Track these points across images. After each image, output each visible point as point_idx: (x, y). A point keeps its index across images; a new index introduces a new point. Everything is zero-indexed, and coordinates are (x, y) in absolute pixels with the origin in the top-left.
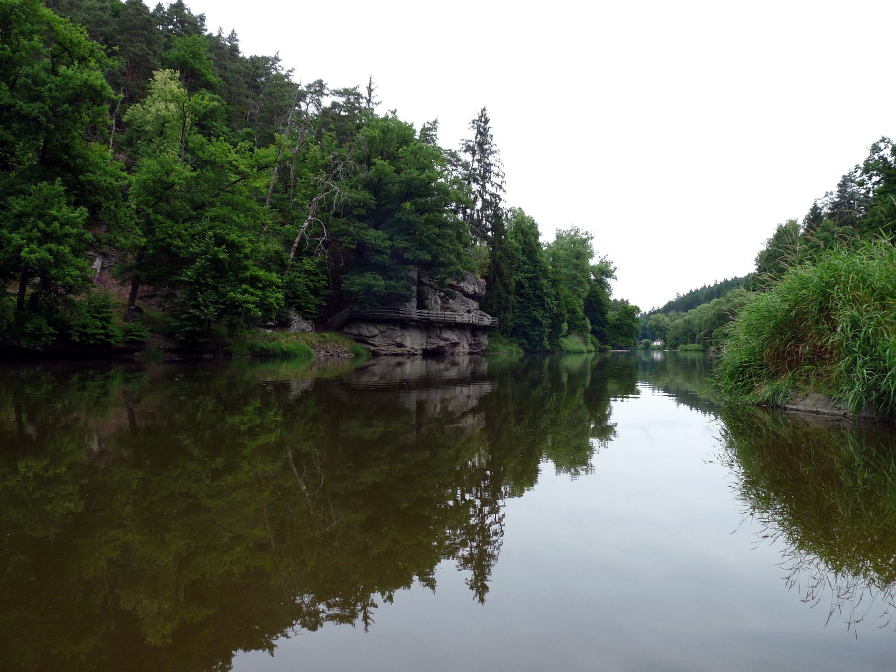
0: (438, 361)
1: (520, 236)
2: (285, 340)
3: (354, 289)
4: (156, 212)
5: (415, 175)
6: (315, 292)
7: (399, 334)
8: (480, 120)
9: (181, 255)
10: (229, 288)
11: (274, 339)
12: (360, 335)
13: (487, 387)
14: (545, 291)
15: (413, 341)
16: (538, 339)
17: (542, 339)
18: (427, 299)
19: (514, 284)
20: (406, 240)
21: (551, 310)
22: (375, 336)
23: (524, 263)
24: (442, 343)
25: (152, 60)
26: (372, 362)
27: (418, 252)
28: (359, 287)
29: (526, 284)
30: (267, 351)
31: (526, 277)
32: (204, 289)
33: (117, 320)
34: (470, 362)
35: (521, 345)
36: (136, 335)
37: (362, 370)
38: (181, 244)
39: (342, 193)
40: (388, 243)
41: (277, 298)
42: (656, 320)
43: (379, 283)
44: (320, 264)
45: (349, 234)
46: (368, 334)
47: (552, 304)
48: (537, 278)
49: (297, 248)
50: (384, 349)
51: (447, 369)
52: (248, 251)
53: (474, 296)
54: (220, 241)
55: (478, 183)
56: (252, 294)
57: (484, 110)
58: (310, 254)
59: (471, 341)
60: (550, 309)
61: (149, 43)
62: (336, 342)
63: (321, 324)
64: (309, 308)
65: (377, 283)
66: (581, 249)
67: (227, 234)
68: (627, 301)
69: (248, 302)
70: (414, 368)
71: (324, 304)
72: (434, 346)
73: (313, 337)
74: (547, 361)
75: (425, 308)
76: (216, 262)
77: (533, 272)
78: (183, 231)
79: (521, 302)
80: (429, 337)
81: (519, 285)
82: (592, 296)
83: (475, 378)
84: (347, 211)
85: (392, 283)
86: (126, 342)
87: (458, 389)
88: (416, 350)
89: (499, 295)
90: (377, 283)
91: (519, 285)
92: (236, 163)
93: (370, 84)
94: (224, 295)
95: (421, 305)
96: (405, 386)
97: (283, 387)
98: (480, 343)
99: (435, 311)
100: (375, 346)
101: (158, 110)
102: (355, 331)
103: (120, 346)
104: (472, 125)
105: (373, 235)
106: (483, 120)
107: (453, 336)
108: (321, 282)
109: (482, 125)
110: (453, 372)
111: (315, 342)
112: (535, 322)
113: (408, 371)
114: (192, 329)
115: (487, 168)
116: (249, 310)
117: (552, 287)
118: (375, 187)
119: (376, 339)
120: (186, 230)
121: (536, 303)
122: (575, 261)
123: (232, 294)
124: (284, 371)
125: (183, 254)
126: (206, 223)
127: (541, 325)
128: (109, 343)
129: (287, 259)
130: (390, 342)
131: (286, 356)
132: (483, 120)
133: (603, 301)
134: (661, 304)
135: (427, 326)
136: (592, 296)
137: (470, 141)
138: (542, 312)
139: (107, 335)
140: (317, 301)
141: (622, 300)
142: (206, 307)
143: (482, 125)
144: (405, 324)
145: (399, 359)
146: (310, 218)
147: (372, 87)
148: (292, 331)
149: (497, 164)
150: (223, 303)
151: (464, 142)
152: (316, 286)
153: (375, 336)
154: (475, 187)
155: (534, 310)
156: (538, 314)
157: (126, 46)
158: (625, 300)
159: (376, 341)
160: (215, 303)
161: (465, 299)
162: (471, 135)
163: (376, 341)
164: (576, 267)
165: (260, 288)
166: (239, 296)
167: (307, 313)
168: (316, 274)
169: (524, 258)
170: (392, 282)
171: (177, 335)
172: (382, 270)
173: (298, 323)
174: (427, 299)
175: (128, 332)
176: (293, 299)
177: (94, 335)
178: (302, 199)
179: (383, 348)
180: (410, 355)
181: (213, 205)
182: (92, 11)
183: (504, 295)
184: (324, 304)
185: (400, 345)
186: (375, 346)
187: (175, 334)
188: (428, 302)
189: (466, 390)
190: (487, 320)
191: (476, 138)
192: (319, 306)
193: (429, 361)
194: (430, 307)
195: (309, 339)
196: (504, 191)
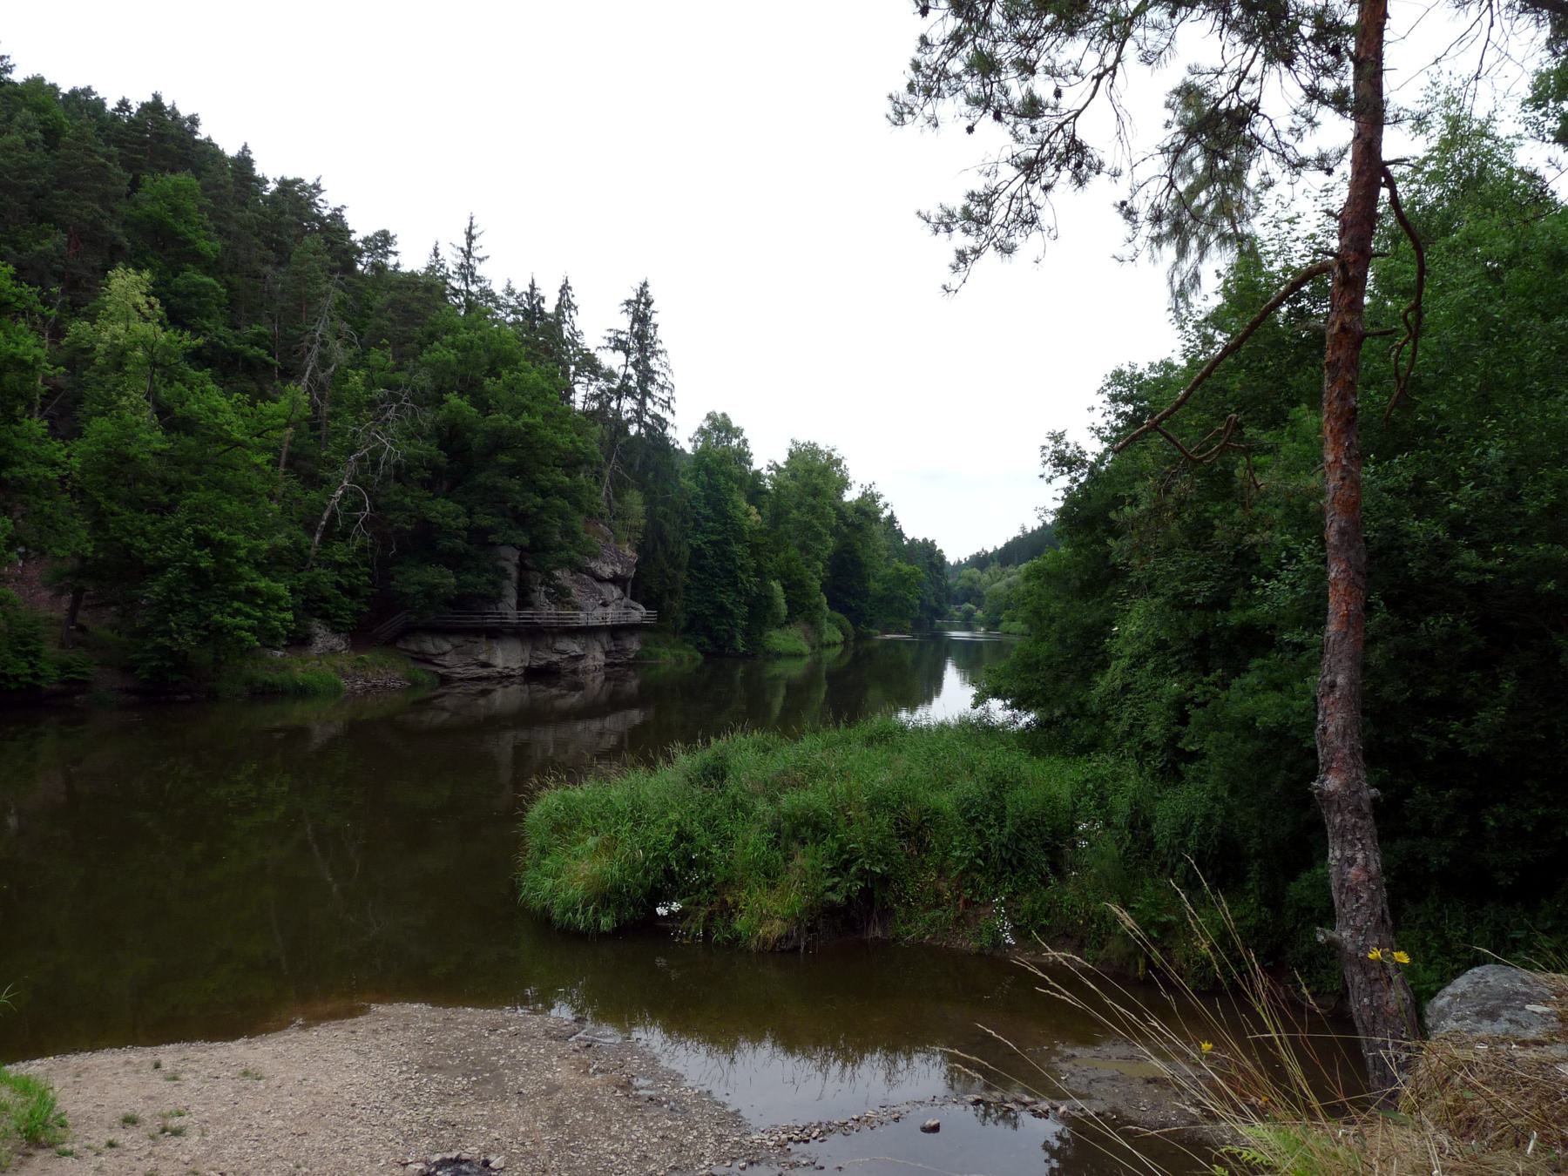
0: (550, 685)
1: (703, 477)
2: (301, 668)
3: (411, 590)
4: (110, 498)
5: (504, 422)
6: (352, 592)
7: (484, 648)
8: (638, 302)
9: (146, 562)
10: (213, 607)
11: (284, 668)
12: (422, 652)
13: (636, 716)
14: (739, 562)
15: (508, 657)
16: (726, 637)
17: (733, 637)
18: (534, 591)
19: (688, 553)
20: (493, 515)
21: (748, 593)
22: (444, 654)
23: (707, 519)
24: (555, 658)
25: (108, 227)
26: (441, 691)
27: (509, 532)
28: (417, 588)
29: (709, 552)
30: (273, 685)
31: (709, 542)
32: (178, 608)
33: (49, 649)
34: (607, 679)
35: (699, 646)
36: (78, 673)
37: (423, 704)
38: (146, 546)
39: (393, 449)
40: (463, 521)
41: (283, 621)
42: (971, 579)
43: (445, 579)
44: (362, 549)
45: (403, 508)
46: (434, 651)
47: (750, 582)
48: (727, 542)
49: (326, 528)
50: (459, 671)
51: (562, 696)
52: (242, 553)
53: (616, 580)
54: (203, 541)
55: (634, 398)
56: (248, 616)
57: (645, 285)
58: (345, 536)
59: (611, 646)
60: (746, 590)
61: (103, 198)
62: (381, 666)
63: (361, 635)
64: (341, 617)
65: (445, 581)
66: (820, 481)
67: (214, 530)
68: (933, 542)
69: (242, 628)
70: (506, 698)
71: (366, 609)
72: (542, 663)
73: (345, 658)
74: (739, 673)
75: (531, 605)
76: (196, 573)
77: (720, 533)
78: (149, 527)
79: (700, 579)
80: (535, 649)
81: (697, 553)
82: (846, 552)
83: (615, 704)
84: (401, 473)
85: (470, 578)
86: (64, 682)
87: (580, 727)
88: (513, 670)
89: (662, 571)
90: (445, 581)
91: (697, 553)
92: (229, 428)
93: (471, 228)
94: (208, 617)
95: (524, 602)
96: (495, 723)
97: (300, 733)
98: (624, 649)
99: (547, 611)
100: (445, 667)
101: (115, 337)
102: (413, 647)
103: (54, 687)
104: (625, 307)
105: (443, 509)
106: (643, 300)
107: (574, 647)
108: (361, 578)
109: (641, 310)
110: (574, 699)
111: (348, 669)
112: (722, 610)
113: (498, 703)
114: (160, 663)
115: (647, 376)
116: (241, 640)
117: (752, 555)
118: (451, 437)
119: (447, 658)
120: (153, 524)
121: (725, 581)
122: (810, 499)
123: (217, 617)
124: (298, 713)
125: (149, 560)
126: (182, 516)
127: (731, 614)
128: (39, 687)
129: (309, 548)
130: (470, 660)
131: (303, 692)
132: (643, 300)
133: (864, 558)
134: (995, 540)
135: (531, 634)
136: (846, 552)
137: (622, 333)
138: (734, 595)
139: (35, 676)
140: (355, 605)
141: (925, 540)
142: (181, 633)
143: (641, 310)
144: (495, 634)
145: (484, 685)
146: (346, 483)
147: (474, 232)
148: (314, 651)
149: (663, 370)
150: (206, 628)
151: (611, 335)
152: (351, 584)
153: (444, 654)
154: (628, 404)
155: (721, 592)
156: (727, 599)
157: (67, 207)
158: (930, 540)
159: (447, 660)
160: (195, 627)
161: (598, 586)
162: (624, 323)
163: (447, 660)
164: (813, 509)
165: (258, 606)
166: (229, 620)
167: (337, 623)
168: (354, 565)
169: (708, 512)
170: (469, 576)
171: (139, 671)
172: (454, 561)
173: (324, 639)
174: (534, 591)
175: (65, 668)
176: (312, 605)
177: (16, 678)
178: (335, 453)
179: (459, 670)
180: (503, 677)
181: (193, 486)
182: (14, 153)
183: (670, 571)
184: (366, 609)
185: (485, 665)
186: (445, 667)
187: (136, 669)
188: (533, 596)
189: (596, 725)
190: (638, 614)
191: (632, 328)
192: (357, 613)
193: (534, 686)
194: (538, 604)
195: (339, 664)
196: (673, 412)
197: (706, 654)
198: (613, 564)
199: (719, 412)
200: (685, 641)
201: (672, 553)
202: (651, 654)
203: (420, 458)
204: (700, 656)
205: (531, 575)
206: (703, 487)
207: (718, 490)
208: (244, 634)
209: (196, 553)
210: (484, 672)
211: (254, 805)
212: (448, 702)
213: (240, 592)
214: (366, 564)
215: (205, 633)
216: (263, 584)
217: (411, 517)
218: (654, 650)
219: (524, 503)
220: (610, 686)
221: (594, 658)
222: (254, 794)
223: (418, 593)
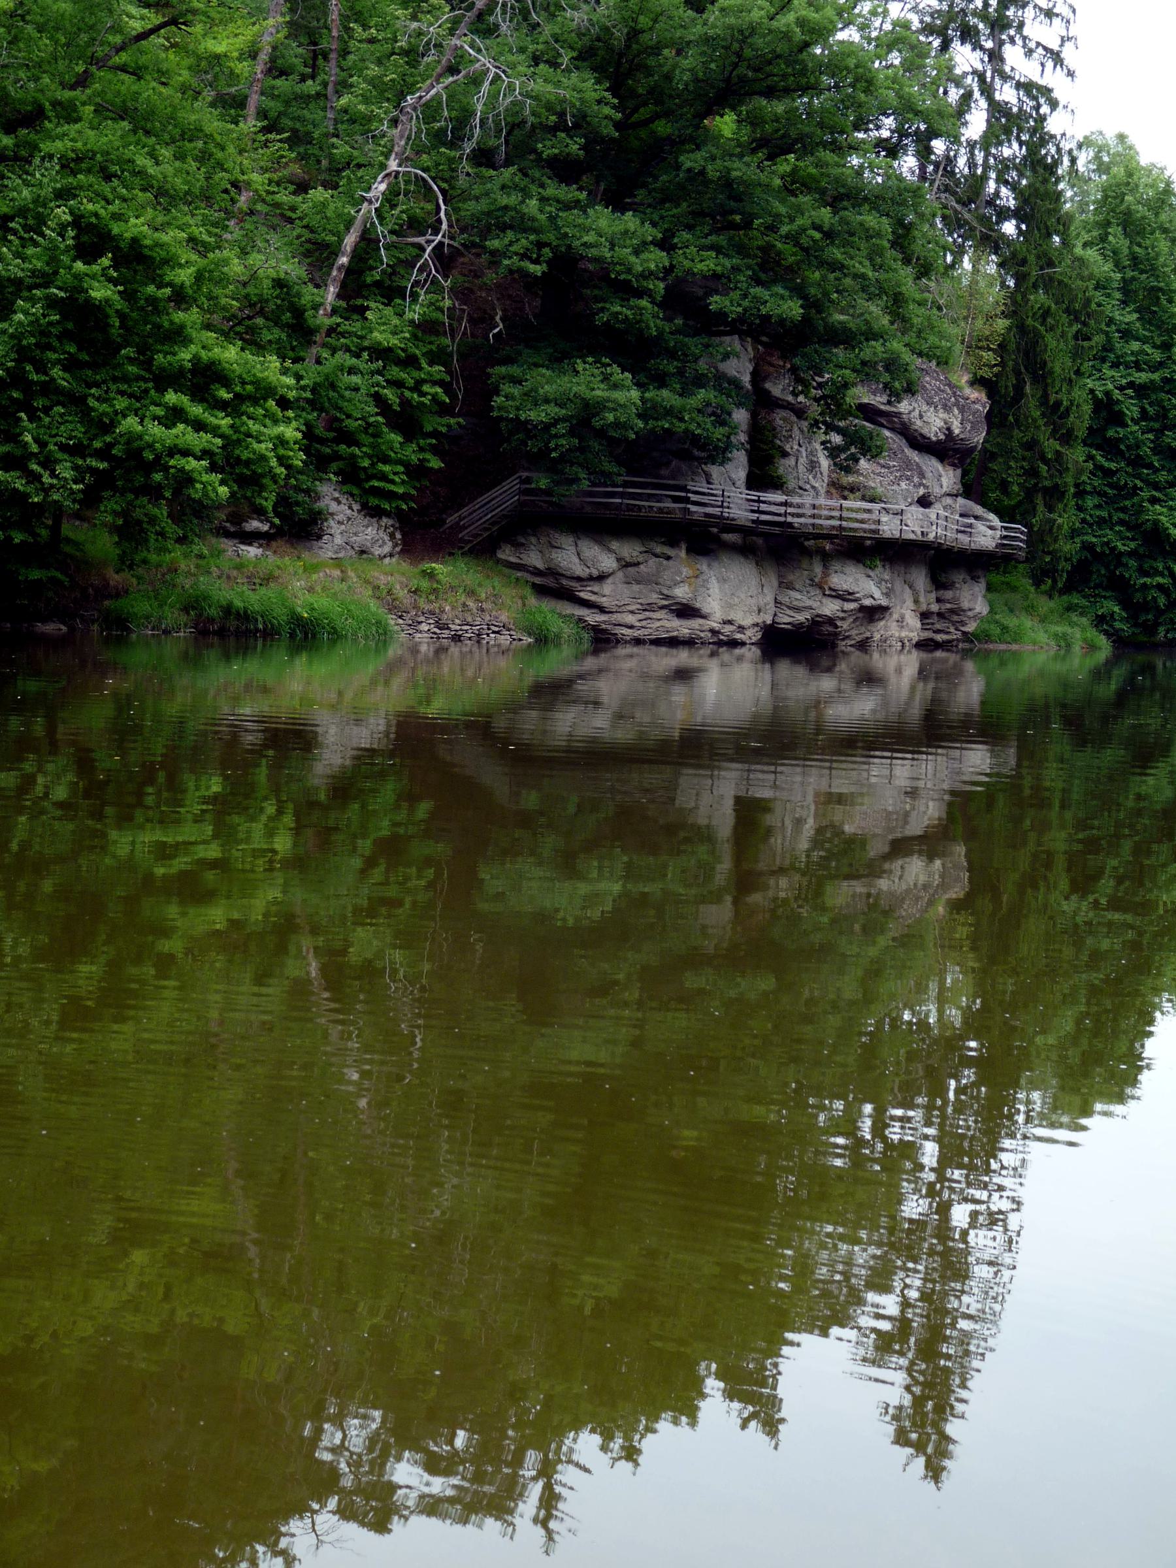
0: (814, 667)
1: (1117, 237)
3: (537, 415)
7: (686, 571)
10: (121, 403)
11: (268, 579)
12: (553, 572)
18: (785, 455)
19: (1087, 408)
22: (601, 578)
23: (1127, 334)
24: (830, 608)
26: (590, 663)
27: (757, 291)
28: (554, 410)
29: (1131, 409)
30: (245, 616)
31: (1131, 385)
32: (39, 403)
34: (923, 674)
35: (1101, 621)
40: (656, 259)
44: (427, 328)
45: (522, 225)
46: (579, 570)
49: (349, 271)
50: (629, 621)
52: (184, 276)
55: (977, 46)
56: (199, 426)
62: (471, 593)
64: (383, 477)
69: (186, 453)
71: (435, 463)
72: (801, 617)
75: (776, 484)
79: (1108, 473)
81: (1107, 410)
88: (741, 629)
89: (1032, 445)
94: (106, 426)
100: (602, 610)
102: (534, 559)
108: (426, 388)
111: (401, 593)
116: (187, 479)
119: (607, 588)
123: (131, 423)
126: (47, 177)
129: (316, 307)
130: (654, 598)
140: (411, 453)
142: (48, 463)
145: (682, 657)
146: (393, 165)
152: (404, 402)
153: (601, 578)
155: (1154, 501)
159: (607, 593)
161: (914, 456)
163: (607, 593)
165: (223, 405)
166: (156, 430)
169: (1129, 317)
170: (665, 393)
174: (785, 455)
178: (366, 100)
179: (630, 619)
180: (720, 643)
181: (69, 113)
183: (1051, 446)
184: (435, 463)
185: (686, 611)
186: (602, 610)
188: (784, 466)
192: (416, 472)
193: (785, 668)
194: (792, 484)
195: (383, 580)
196: (1071, 74)
197: (1119, 641)
198: (947, 408)
199: (1110, 135)
200: (1070, 608)
201: (1058, 404)
202: (1005, 629)
203: (556, 108)
204: (1103, 641)
205: (779, 418)
206: (1118, 265)
207: (1153, 270)
208: (192, 464)
209: (79, 266)
210: (683, 628)
211: (210, 876)
212: (609, 689)
213: (181, 371)
214: (434, 358)
215: (102, 465)
216: (230, 354)
217: (540, 245)
218: (1012, 622)
219: (792, 220)
220: (926, 690)
221: (901, 621)
222: (213, 852)
223: (556, 421)
